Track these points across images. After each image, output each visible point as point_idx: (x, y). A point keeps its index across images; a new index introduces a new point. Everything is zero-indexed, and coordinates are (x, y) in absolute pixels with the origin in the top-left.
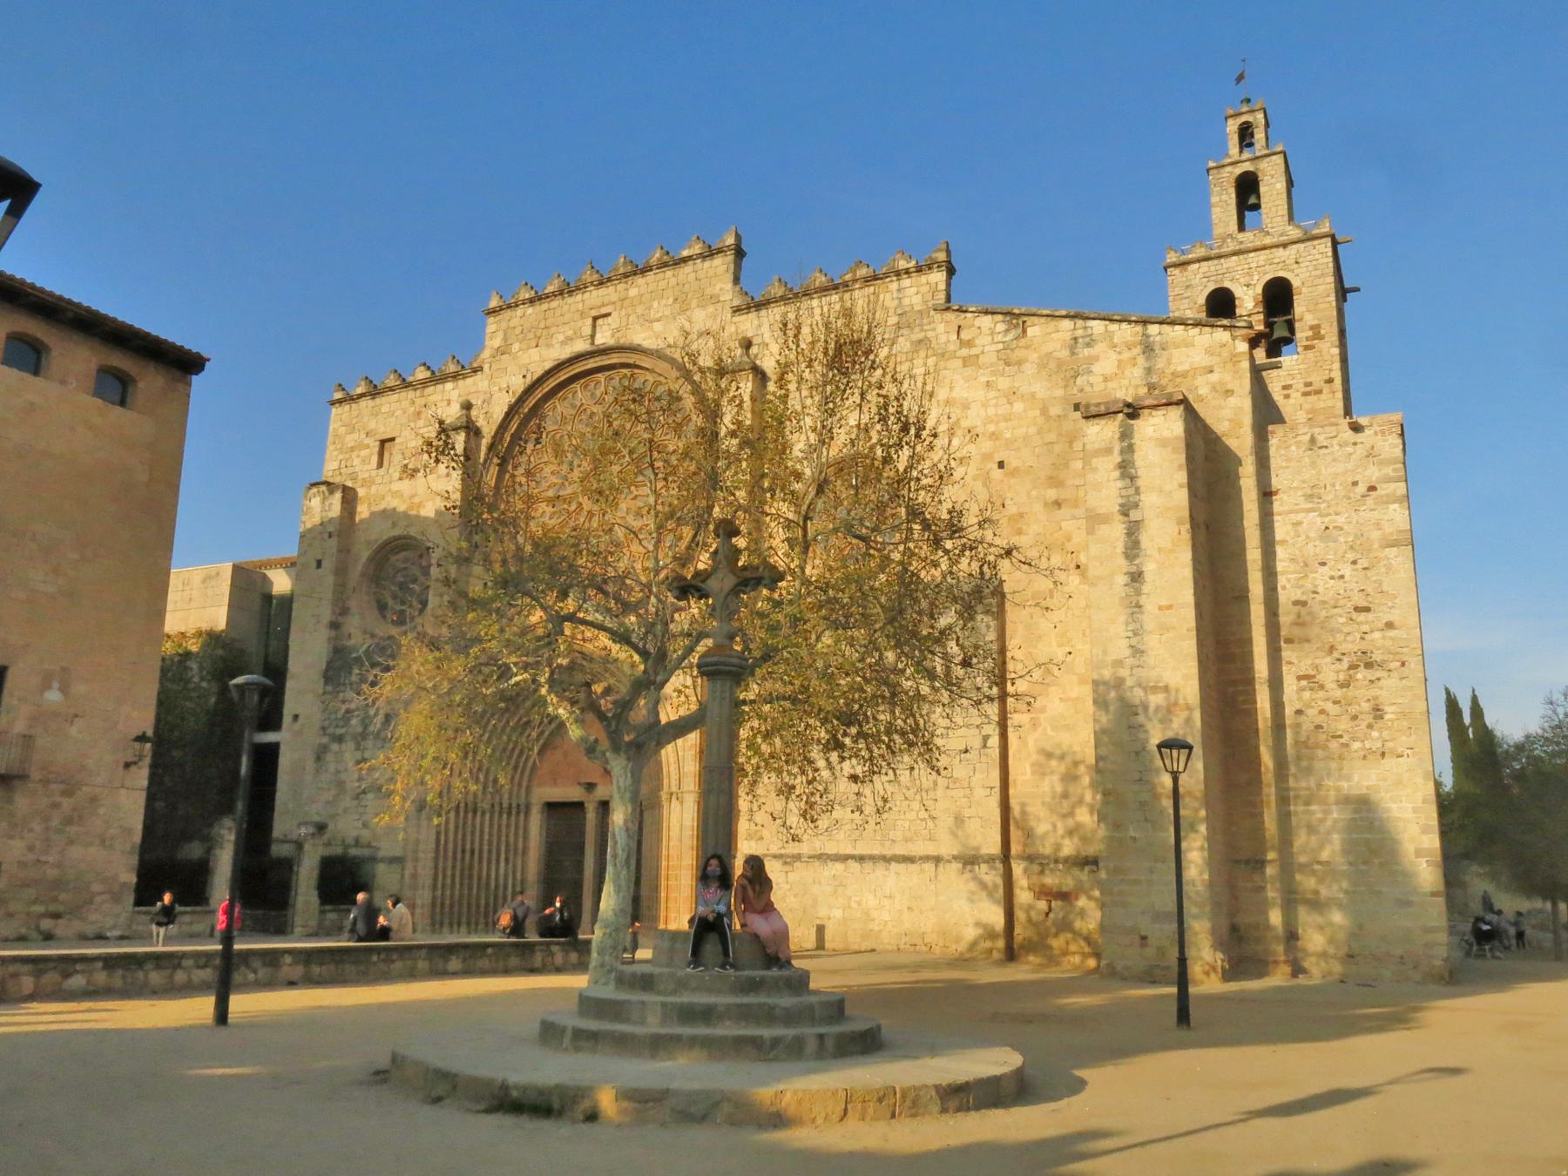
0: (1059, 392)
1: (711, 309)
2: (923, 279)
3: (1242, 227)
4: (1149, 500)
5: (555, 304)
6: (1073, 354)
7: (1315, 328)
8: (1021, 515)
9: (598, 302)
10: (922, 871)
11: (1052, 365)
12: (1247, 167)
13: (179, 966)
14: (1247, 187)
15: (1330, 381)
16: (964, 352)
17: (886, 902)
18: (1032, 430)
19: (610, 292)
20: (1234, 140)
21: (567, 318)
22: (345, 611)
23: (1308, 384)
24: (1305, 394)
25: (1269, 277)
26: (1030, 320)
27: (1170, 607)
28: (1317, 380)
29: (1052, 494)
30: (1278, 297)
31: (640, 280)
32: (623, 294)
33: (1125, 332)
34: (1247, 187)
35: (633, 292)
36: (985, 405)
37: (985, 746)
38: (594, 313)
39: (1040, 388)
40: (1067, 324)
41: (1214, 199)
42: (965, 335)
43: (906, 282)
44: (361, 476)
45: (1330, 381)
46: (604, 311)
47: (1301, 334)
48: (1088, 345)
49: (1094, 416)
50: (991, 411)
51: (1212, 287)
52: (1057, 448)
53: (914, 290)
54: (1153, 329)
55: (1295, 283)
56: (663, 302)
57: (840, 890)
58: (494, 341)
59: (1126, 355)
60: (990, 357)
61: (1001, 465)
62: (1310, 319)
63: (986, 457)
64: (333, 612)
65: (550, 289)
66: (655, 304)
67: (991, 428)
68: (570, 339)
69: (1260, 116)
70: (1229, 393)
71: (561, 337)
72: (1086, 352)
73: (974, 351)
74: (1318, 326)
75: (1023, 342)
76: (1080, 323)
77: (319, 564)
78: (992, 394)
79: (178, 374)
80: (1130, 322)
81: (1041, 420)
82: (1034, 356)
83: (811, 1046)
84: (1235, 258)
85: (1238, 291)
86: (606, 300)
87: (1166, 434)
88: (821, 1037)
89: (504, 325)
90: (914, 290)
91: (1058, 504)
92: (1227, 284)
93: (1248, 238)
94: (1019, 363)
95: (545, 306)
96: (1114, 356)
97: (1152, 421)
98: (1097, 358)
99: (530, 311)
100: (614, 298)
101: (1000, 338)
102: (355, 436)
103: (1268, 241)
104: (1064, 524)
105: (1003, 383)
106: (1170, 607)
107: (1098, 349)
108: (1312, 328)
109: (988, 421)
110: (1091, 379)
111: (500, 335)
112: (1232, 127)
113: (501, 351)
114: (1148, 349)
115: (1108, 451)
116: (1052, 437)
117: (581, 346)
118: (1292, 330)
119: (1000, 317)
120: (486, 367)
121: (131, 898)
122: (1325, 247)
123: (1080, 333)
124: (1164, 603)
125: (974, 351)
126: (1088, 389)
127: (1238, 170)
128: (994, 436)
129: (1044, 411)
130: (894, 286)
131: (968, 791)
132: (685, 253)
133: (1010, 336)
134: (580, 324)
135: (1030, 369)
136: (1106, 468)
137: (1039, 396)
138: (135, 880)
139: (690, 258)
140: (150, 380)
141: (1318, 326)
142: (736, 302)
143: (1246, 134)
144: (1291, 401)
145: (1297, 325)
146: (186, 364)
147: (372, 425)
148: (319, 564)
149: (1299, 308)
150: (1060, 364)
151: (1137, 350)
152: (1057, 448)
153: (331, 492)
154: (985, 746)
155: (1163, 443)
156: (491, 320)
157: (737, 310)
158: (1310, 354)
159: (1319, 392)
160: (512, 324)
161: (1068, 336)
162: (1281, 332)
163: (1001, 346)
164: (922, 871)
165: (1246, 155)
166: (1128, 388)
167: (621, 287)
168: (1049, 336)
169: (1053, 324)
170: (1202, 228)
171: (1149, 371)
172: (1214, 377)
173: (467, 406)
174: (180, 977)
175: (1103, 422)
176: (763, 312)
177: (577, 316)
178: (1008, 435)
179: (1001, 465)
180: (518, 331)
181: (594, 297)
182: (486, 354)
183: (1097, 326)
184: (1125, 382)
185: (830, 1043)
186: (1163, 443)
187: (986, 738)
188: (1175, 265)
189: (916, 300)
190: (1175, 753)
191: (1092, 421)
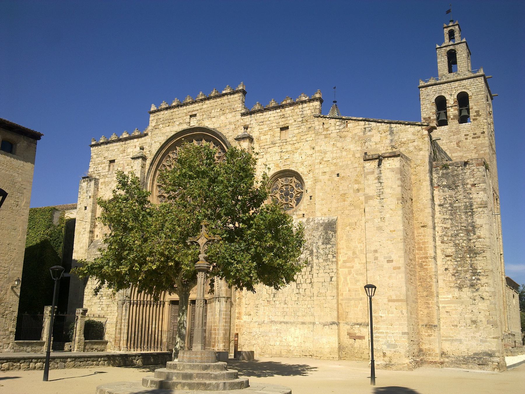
0: (359, 148)
1: (234, 113)
2: (311, 104)
3: (450, 71)
4: (387, 191)
5: (175, 110)
6: (364, 134)
7: (477, 112)
8: (345, 194)
9: (191, 110)
10: (309, 328)
11: (357, 138)
12: (451, 47)
13: (31, 362)
14: (452, 57)
15: (483, 133)
16: (325, 133)
17: (296, 339)
18: (349, 162)
19: (196, 106)
20: (447, 37)
21: (180, 115)
22: (95, 226)
23: (475, 134)
24: (473, 138)
25: (459, 92)
26: (349, 121)
27: (394, 231)
28: (478, 132)
29: (356, 186)
30: (463, 100)
31: (207, 102)
32: (201, 107)
33: (384, 126)
34: (452, 57)
35: (205, 106)
36: (332, 153)
37: (331, 281)
38: (190, 114)
39: (352, 147)
40: (362, 123)
41: (438, 60)
42: (325, 126)
43: (305, 105)
44: (102, 174)
45: (483, 133)
46: (194, 113)
47: (472, 114)
48: (370, 131)
49: (368, 160)
50: (335, 155)
51: (437, 95)
52: (358, 169)
53: (308, 108)
54: (393, 126)
55: (470, 94)
56: (216, 110)
57: (279, 334)
58: (152, 124)
59: (384, 135)
60: (334, 135)
61: (338, 175)
62: (475, 108)
63: (332, 172)
64: (91, 227)
65: (174, 104)
66: (213, 111)
67: (335, 161)
68: (181, 123)
69: (457, 27)
70: (421, 150)
71: (178, 123)
72: (369, 133)
73: (329, 132)
74: (479, 111)
75: (346, 129)
76: (367, 123)
77: (86, 208)
78: (335, 149)
79: (32, 140)
80: (385, 123)
81: (352, 159)
82: (350, 135)
83: (221, 385)
84: (446, 84)
85: (447, 97)
86: (195, 109)
87: (393, 166)
88: (225, 383)
89: (156, 117)
90: (308, 108)
91: (358, 190)
92: (443, 94)
93: (452, 76)
94: (345, 137)
95: (172, 111)
96: (379, 135)
97: (388, 162)
98: (373, 136)
99: (166, 112)
100: (198, 108)
101: (337, 127)
102: (100, 159)
103: (459, 78)
104: (360, 197)
105: (339, 145)
106: (394, 231)
107: (374, 132)
108: (476, 112)
109: (333, 159)
110: (371, 144)
111: (155, 121)
112: (446, 31)
113: (155, 128)
114: (392, 133)
115: (373, 172)
116: (356, 165)
117: (185, 127)
118: (469, 113)
119: (338, 120)
120: (149, 133)
121: (13, 336)
122: (482, 80)
123: (366, 126)
124: (392, 229)
125: (329, 132)
126: (369, 147)
127: (448, 49)
128: (336, 165)
129: (354, 155)
130: (300, 106)
131: (325, 298)
132: (224, 92)
133: (342, 127)
134: (185, 118)
135: (348, 139)
136: (372, 178)
137: (352, 150)
138: (15, 330)
139: (226, 94)
140: (22, 144)
141: (479, 111)
142: (243, 111)
143: (451, 34)
144: (468, 141)
145: (470, 110)
146: (35, 136)
147: (106, 155)
148: (86, 208)
149: (471, 104)
150: (360, 137)
151: (388, 133)
152: (358, 169)
153: (90, 181)
154: (331, 281)
155: (392, 170)
156: (151, 115)
157: (243, 115)
158: (475, 122)
159: (480, 137)
160: (159, 117)
161: (363, 127)
162: (464, 113)
163: (338, 131)
164: (309, 328)
165: (451, 43)
166: (383, 149)
167: (200, 104)
168: (356, 127)
169: (356, 123)
170: (435, 73)
171: (392, 140)
172: (415, 144)
173: (142, 148)
174: (32, 365)
175: (371, 162)
176: (253, 115)
177: (184, 115)
178: (341, 164)
179: (338, 175)
180: (161, 120)
181: (190, 108)
182: (150, 128)
183: (373, 124)
184: (383, 145)
185: (227, 385)
186: (392, 170)
187: (331, 278)
188: (423, 87)
189: (309, 112)
190: (370, 289)
191: (367, 162)
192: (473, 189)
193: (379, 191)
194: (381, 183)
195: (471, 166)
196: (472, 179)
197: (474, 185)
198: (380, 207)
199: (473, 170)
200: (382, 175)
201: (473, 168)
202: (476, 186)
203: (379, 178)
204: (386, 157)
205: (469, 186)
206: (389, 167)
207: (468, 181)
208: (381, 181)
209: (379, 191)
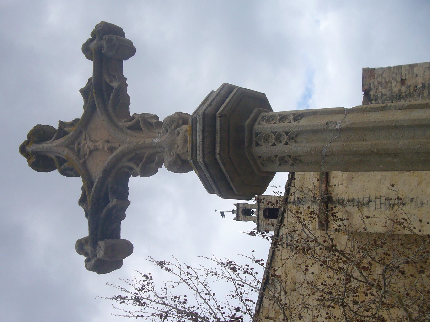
127: (262, 217)
155: (350, 180)
192: (408, 83)
193: (383, 206)
194: (370, 201)
195: (372, 87)
196: (394, 84)
197: (403, 82)
198: (413, 205)
199: (380, 83)
200: (356, 197)
201: (376, 83)
202: (404, 78)
203: (361, 204)
204: (327, 189)
205: (403, 89)
206: (345, 185)
207: (395, 90)
208: (366, 200)
209: (383, 206)
